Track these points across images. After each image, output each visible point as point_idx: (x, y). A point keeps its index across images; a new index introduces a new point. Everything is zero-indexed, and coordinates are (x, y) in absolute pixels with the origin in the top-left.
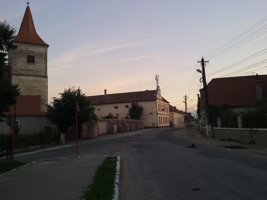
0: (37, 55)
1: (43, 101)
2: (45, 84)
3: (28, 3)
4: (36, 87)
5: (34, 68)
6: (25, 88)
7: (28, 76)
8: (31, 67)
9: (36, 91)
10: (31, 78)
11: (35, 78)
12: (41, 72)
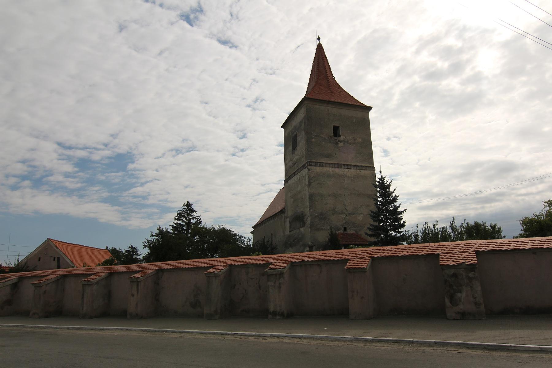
3: (319, 39)
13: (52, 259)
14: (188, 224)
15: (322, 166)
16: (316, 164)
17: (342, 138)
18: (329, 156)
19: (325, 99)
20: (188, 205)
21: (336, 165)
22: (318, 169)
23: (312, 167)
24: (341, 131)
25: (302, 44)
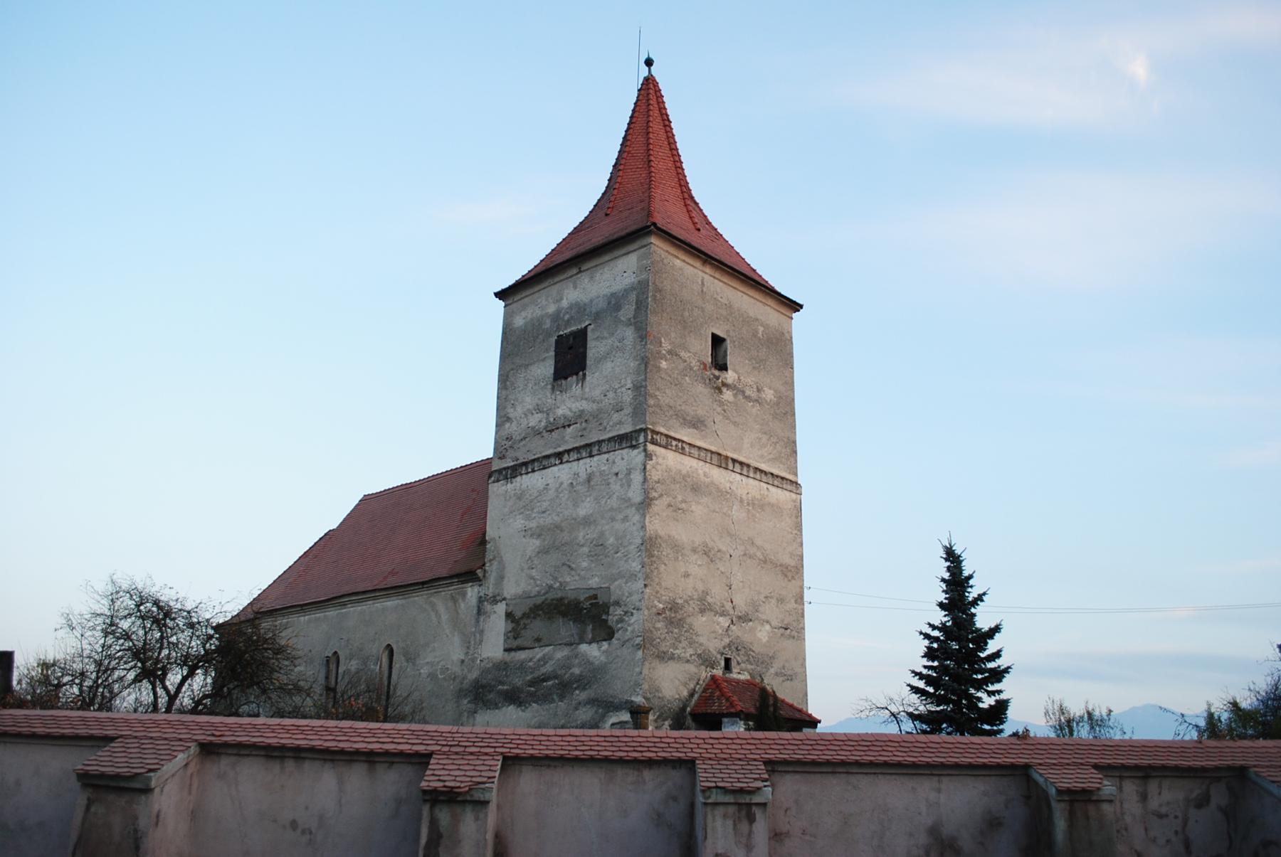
0: (597, 316)
1: (619, 611)
2: (630, 494)
3: (649, 63)
4: (587, 522)
5: (584, 405)
6: (537, 542)
7: (552, 460)
8: (570, 402)
9: (585, 549)
10: (561, 473)
11: (583, 467)
12: (616, 417)
18: (697, 423)
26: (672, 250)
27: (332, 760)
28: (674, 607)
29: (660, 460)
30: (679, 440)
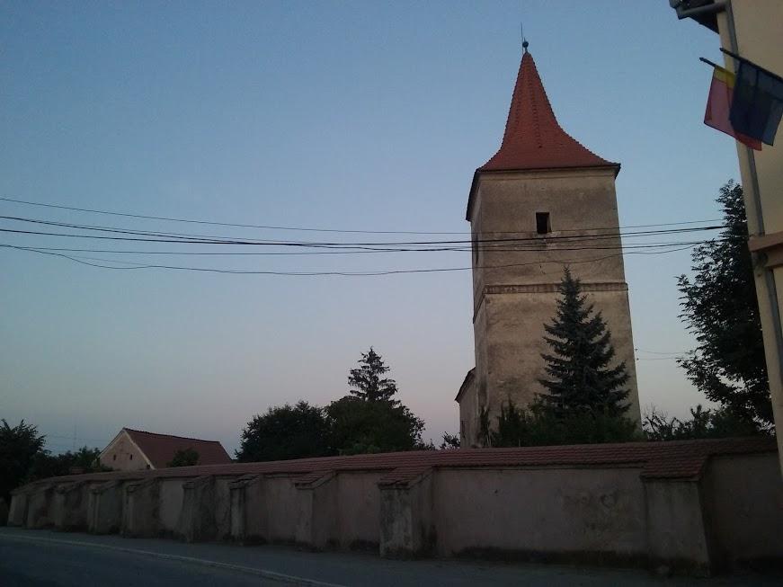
3: (525, 45)
13: (129, 456)
14: (372, 391)
15: (514, 292)
16: (501, 289)
17: (554, 234)
18: (526, 272)
19: (316, 242)
20: (372, 357)
21: (541, 288)
22: (505, 298)
23: (493, 296)
24: (552, 222)
25: (525, 45)
26: (498, 177)
27: (273, 478)
28: (513, 381)
29: (496, 302)
30: (510, 286)
